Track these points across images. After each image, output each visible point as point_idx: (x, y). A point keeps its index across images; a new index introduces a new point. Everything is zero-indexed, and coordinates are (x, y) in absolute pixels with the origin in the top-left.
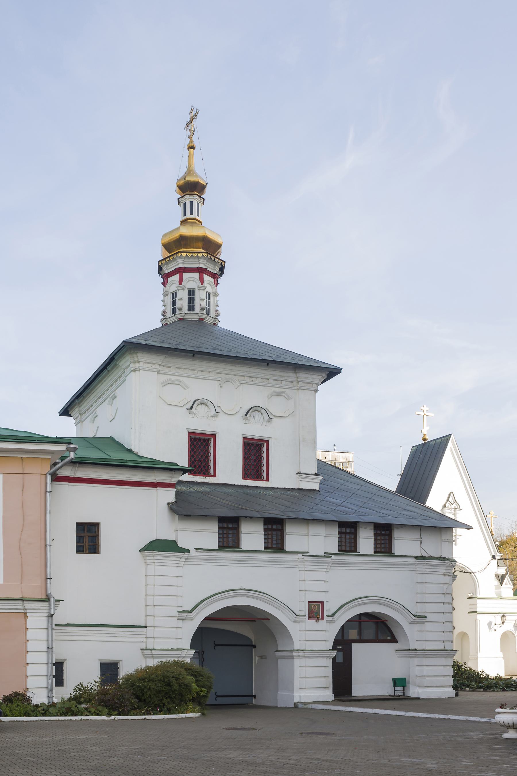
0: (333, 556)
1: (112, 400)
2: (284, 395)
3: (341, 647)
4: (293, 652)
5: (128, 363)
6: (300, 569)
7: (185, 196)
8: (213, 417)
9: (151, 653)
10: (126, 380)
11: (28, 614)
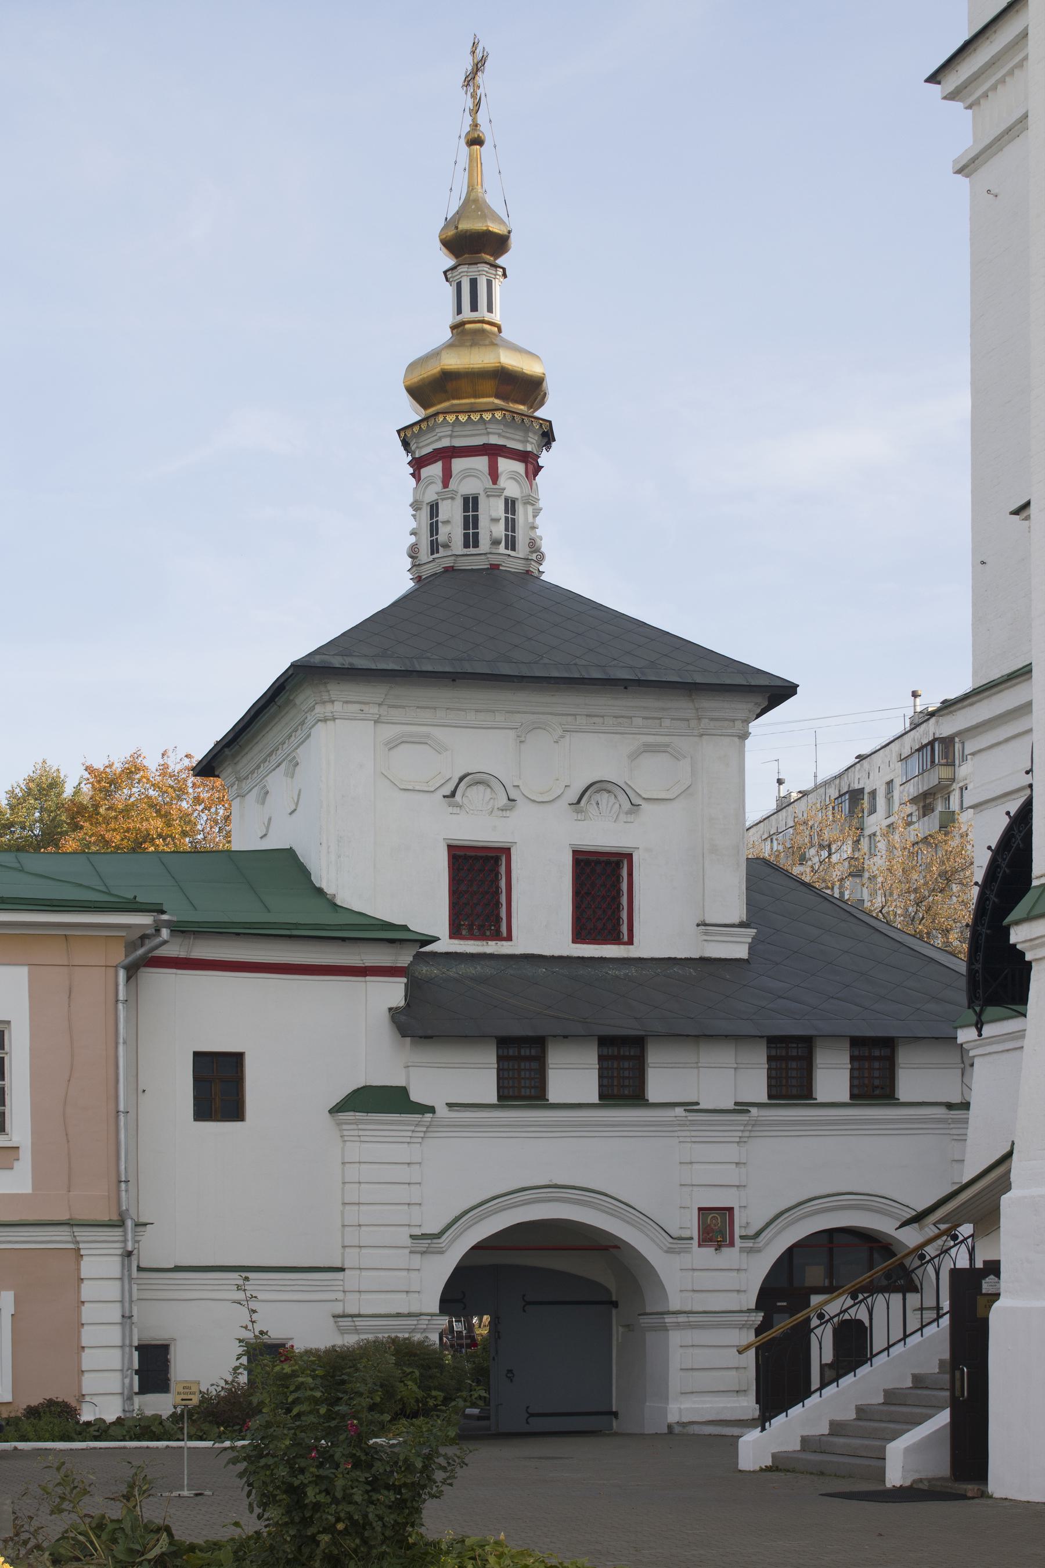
0: (754, 1111)
2: (669, 749)
3: (785, 1304)
4: (665, 1316)
5: (311, 702)
6: (681, 1139)
7: (458, 268)
8: (504, 812)
9: (352, 1324)
10: (309, 736)
11: (82, 1252)
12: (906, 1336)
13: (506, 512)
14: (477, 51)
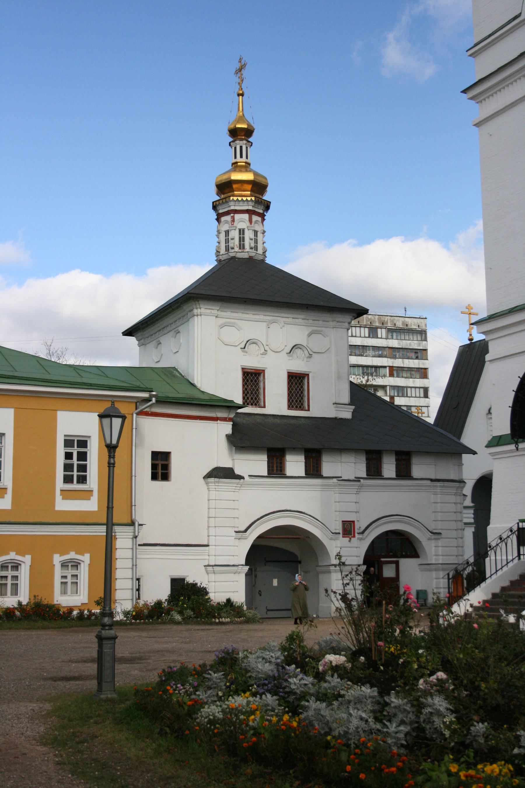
0: (362, 480)
1: (175, 334)
6: (336, 492)
11: (117, 537)
12: (497, 571)
13: (255, 236)
14: (242, 61)
